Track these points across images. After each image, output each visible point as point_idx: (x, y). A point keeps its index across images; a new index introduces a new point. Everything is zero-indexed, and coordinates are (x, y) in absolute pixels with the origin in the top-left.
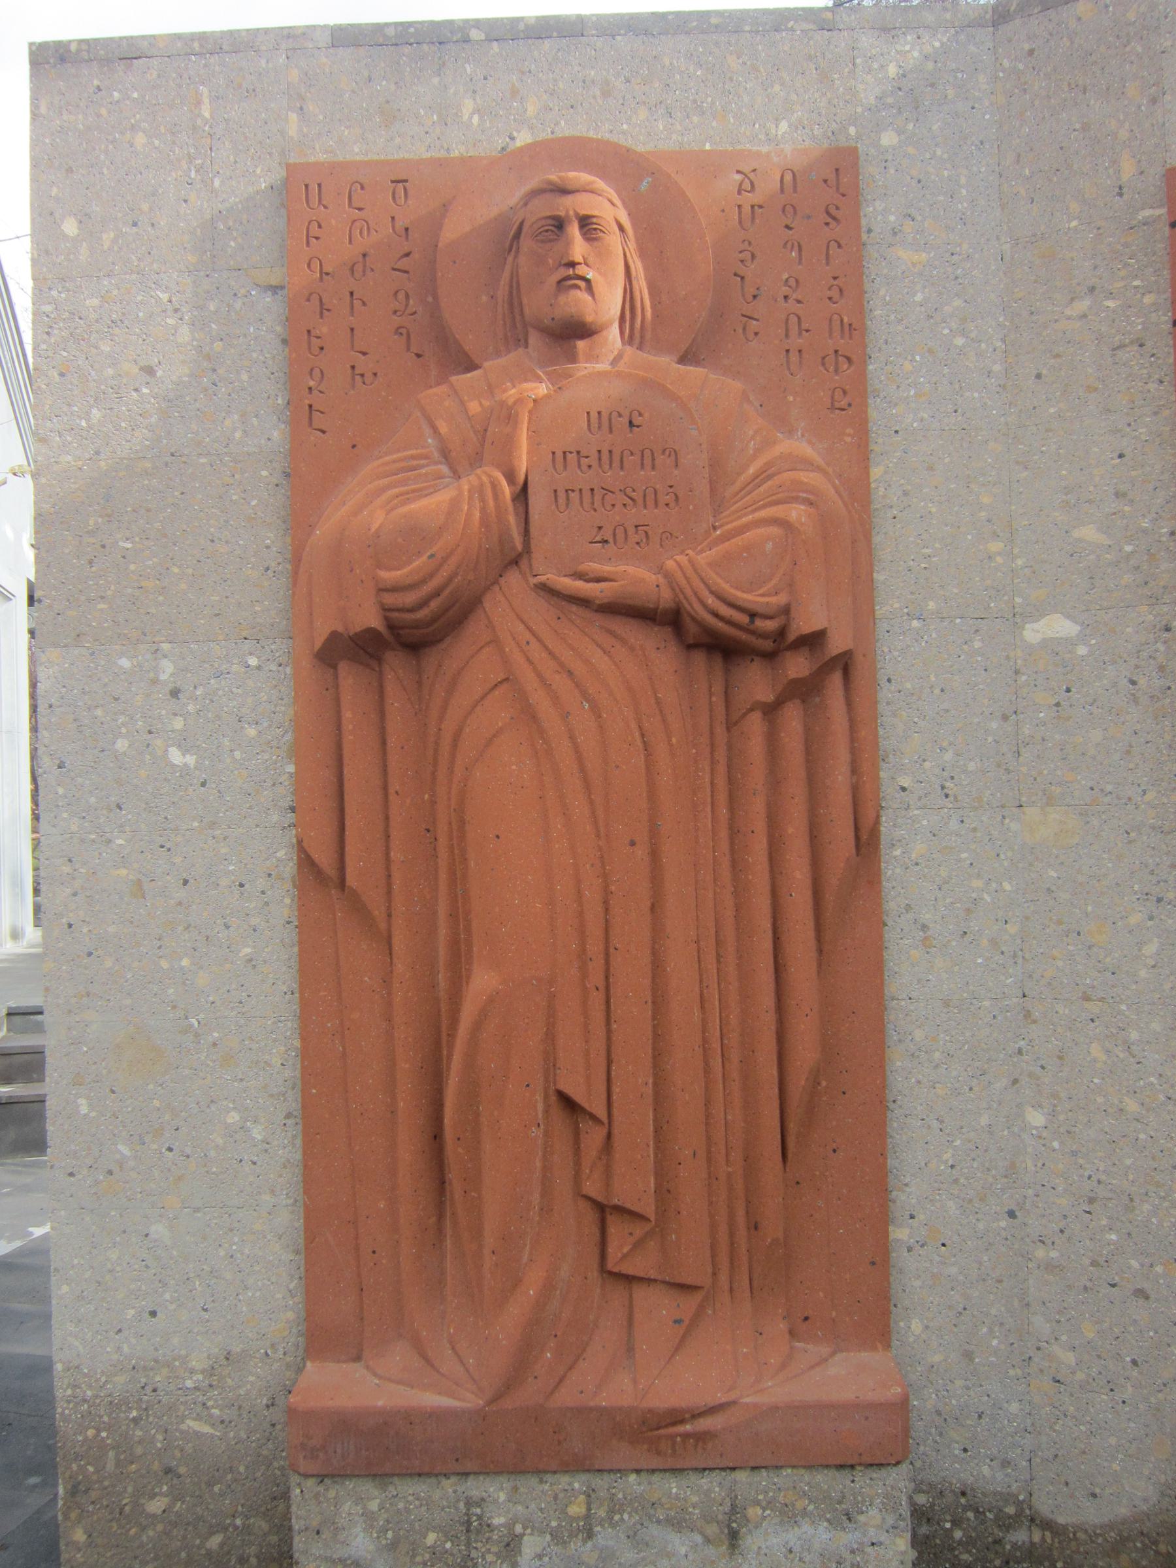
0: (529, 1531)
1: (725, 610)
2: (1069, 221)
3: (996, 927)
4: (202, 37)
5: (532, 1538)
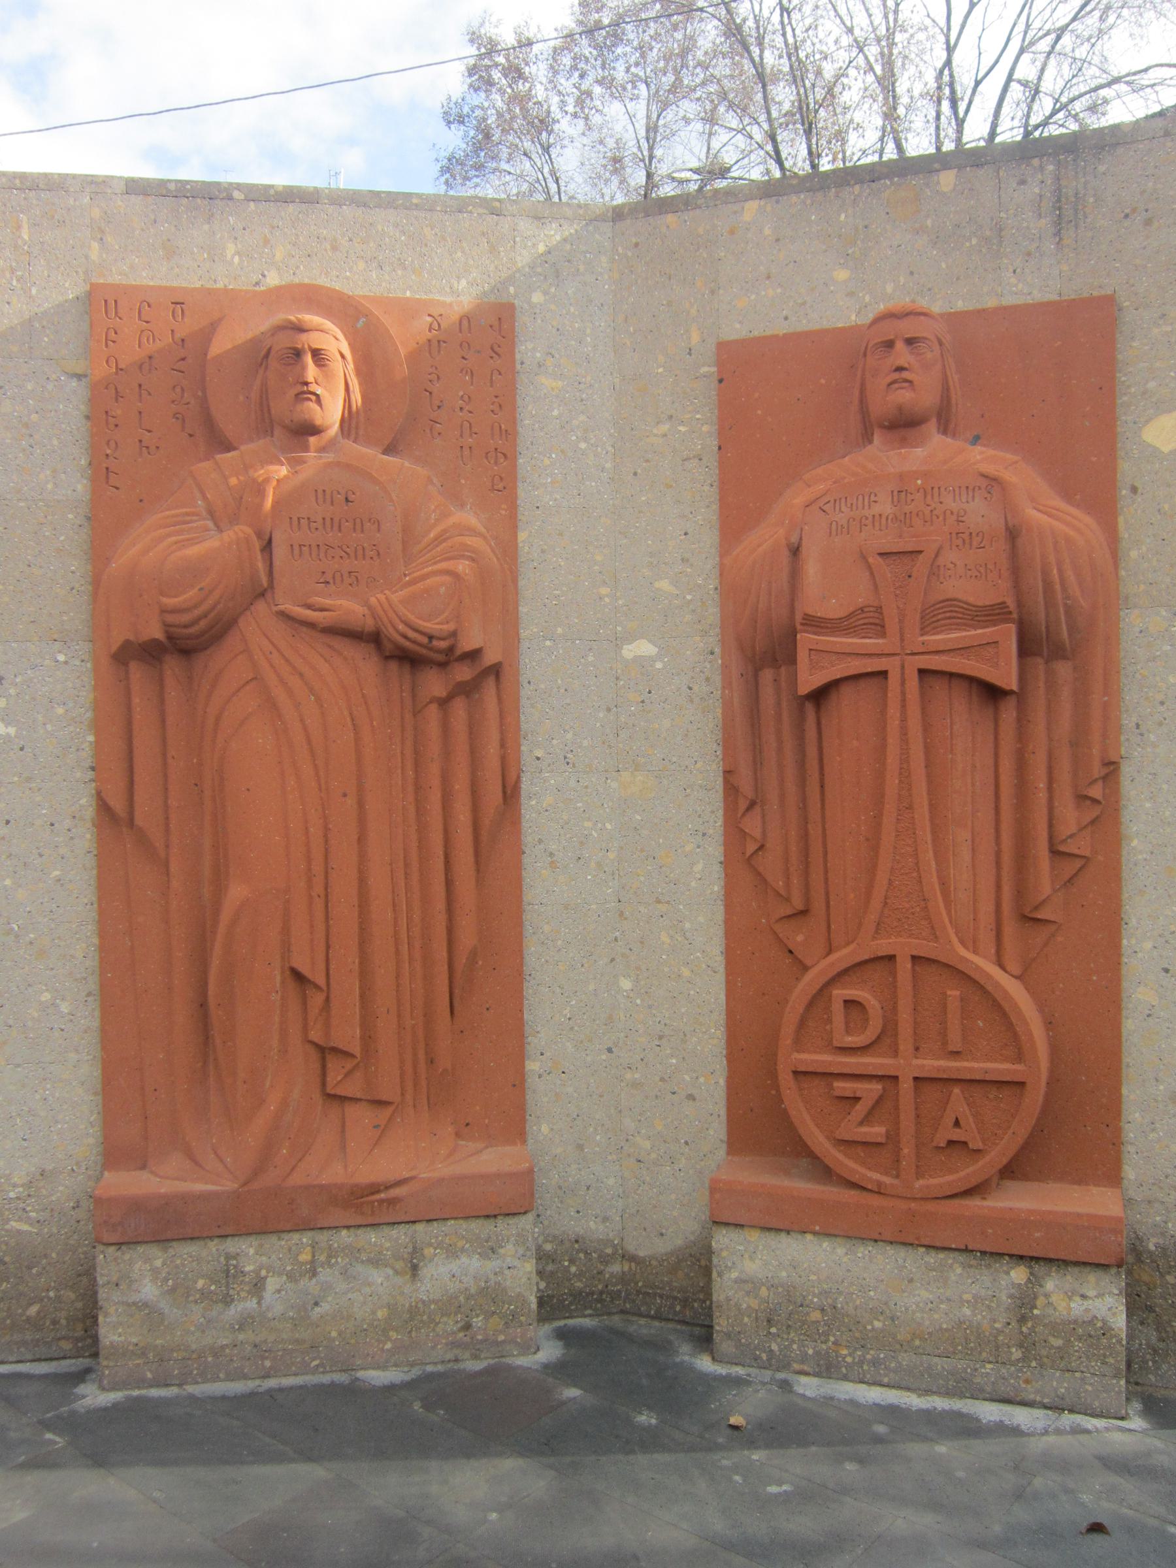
0: (271, 1274)
1: (412, 634)
2: (658, 368)
3: (601, 854)
4: (23, 176)
5: (273, 1279)
